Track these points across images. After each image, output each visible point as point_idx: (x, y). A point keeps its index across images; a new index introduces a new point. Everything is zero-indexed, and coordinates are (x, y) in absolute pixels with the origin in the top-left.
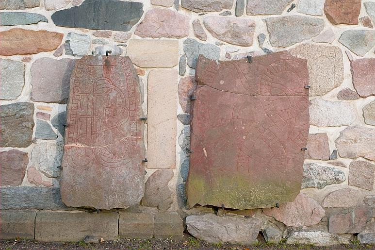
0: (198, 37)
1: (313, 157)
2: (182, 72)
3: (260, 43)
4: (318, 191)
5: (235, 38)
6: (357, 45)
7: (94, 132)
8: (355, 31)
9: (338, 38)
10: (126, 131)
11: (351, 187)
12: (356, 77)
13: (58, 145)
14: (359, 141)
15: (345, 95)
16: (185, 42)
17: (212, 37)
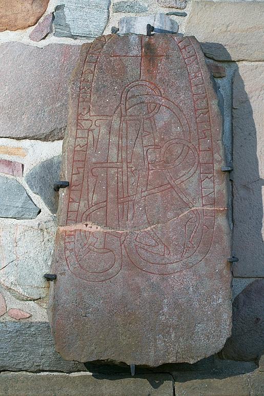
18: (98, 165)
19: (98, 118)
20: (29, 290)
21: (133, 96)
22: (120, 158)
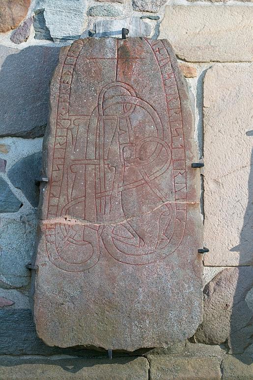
7: (100, 193)
10: (166, 190)
13: (23, 222)
18: (77, 162)
19: (76, 117)
20: (12, 280)
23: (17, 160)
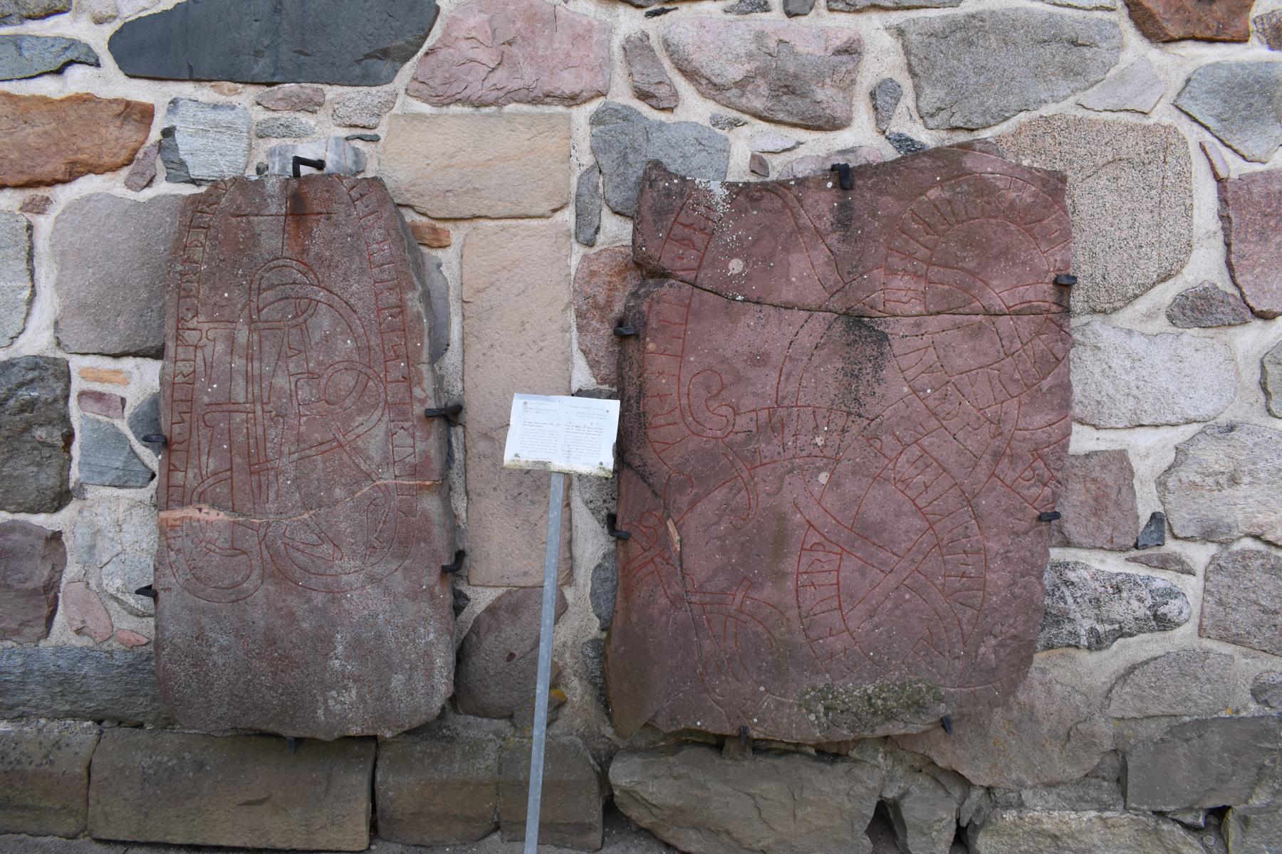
0: (643, 96)
1: (1076, 538)
2: (586, 233)
3: (880, 114)
4: (1088, 659)
5: (784, 98)
6: (1245, 119)
8: (1239, 65)
9: (1172, 94)
11: (1208, 644)
12: (1242, 241)
14: (1247, 479)
15: (1197, 310)
16: (596, 120)
17: (697, 97)
18: (213, 408)
19: (212, 325)
21: (272, 287)
22: (250, 396)
23: (142, 398)
